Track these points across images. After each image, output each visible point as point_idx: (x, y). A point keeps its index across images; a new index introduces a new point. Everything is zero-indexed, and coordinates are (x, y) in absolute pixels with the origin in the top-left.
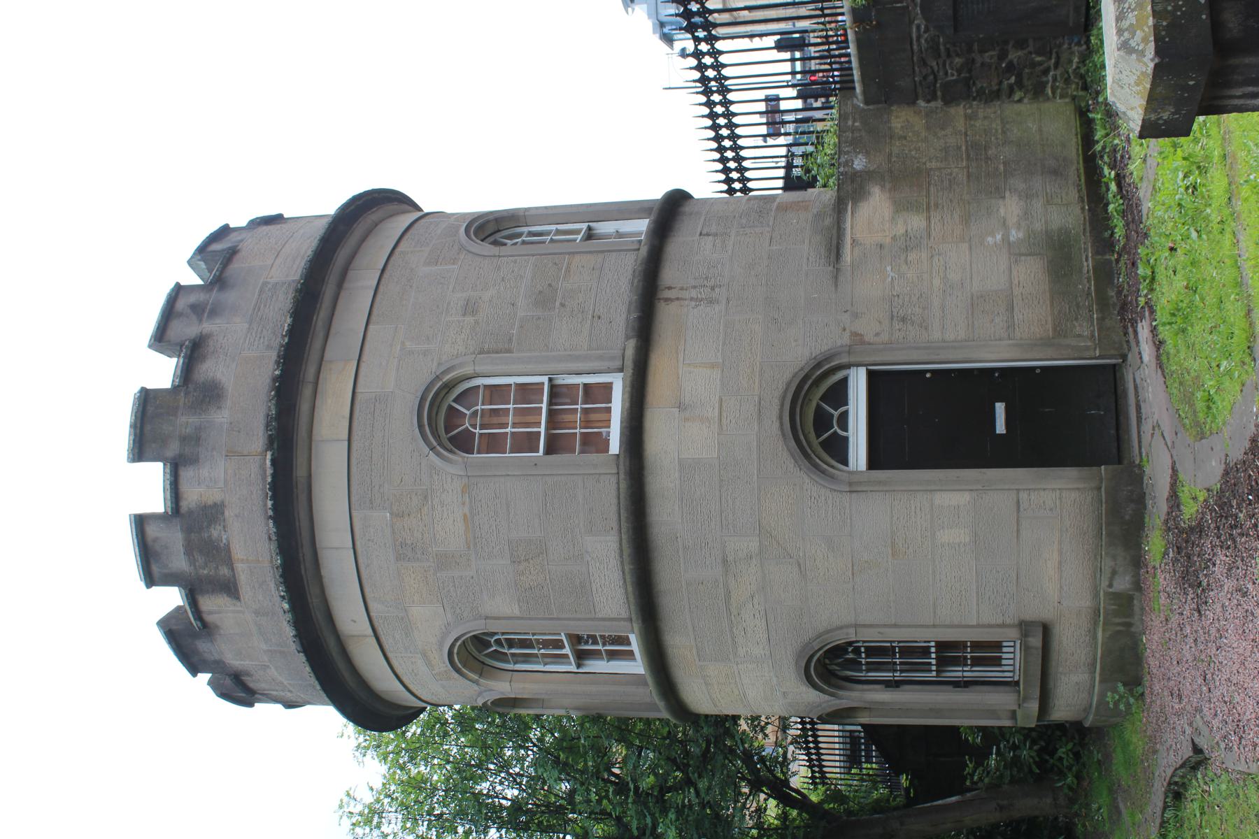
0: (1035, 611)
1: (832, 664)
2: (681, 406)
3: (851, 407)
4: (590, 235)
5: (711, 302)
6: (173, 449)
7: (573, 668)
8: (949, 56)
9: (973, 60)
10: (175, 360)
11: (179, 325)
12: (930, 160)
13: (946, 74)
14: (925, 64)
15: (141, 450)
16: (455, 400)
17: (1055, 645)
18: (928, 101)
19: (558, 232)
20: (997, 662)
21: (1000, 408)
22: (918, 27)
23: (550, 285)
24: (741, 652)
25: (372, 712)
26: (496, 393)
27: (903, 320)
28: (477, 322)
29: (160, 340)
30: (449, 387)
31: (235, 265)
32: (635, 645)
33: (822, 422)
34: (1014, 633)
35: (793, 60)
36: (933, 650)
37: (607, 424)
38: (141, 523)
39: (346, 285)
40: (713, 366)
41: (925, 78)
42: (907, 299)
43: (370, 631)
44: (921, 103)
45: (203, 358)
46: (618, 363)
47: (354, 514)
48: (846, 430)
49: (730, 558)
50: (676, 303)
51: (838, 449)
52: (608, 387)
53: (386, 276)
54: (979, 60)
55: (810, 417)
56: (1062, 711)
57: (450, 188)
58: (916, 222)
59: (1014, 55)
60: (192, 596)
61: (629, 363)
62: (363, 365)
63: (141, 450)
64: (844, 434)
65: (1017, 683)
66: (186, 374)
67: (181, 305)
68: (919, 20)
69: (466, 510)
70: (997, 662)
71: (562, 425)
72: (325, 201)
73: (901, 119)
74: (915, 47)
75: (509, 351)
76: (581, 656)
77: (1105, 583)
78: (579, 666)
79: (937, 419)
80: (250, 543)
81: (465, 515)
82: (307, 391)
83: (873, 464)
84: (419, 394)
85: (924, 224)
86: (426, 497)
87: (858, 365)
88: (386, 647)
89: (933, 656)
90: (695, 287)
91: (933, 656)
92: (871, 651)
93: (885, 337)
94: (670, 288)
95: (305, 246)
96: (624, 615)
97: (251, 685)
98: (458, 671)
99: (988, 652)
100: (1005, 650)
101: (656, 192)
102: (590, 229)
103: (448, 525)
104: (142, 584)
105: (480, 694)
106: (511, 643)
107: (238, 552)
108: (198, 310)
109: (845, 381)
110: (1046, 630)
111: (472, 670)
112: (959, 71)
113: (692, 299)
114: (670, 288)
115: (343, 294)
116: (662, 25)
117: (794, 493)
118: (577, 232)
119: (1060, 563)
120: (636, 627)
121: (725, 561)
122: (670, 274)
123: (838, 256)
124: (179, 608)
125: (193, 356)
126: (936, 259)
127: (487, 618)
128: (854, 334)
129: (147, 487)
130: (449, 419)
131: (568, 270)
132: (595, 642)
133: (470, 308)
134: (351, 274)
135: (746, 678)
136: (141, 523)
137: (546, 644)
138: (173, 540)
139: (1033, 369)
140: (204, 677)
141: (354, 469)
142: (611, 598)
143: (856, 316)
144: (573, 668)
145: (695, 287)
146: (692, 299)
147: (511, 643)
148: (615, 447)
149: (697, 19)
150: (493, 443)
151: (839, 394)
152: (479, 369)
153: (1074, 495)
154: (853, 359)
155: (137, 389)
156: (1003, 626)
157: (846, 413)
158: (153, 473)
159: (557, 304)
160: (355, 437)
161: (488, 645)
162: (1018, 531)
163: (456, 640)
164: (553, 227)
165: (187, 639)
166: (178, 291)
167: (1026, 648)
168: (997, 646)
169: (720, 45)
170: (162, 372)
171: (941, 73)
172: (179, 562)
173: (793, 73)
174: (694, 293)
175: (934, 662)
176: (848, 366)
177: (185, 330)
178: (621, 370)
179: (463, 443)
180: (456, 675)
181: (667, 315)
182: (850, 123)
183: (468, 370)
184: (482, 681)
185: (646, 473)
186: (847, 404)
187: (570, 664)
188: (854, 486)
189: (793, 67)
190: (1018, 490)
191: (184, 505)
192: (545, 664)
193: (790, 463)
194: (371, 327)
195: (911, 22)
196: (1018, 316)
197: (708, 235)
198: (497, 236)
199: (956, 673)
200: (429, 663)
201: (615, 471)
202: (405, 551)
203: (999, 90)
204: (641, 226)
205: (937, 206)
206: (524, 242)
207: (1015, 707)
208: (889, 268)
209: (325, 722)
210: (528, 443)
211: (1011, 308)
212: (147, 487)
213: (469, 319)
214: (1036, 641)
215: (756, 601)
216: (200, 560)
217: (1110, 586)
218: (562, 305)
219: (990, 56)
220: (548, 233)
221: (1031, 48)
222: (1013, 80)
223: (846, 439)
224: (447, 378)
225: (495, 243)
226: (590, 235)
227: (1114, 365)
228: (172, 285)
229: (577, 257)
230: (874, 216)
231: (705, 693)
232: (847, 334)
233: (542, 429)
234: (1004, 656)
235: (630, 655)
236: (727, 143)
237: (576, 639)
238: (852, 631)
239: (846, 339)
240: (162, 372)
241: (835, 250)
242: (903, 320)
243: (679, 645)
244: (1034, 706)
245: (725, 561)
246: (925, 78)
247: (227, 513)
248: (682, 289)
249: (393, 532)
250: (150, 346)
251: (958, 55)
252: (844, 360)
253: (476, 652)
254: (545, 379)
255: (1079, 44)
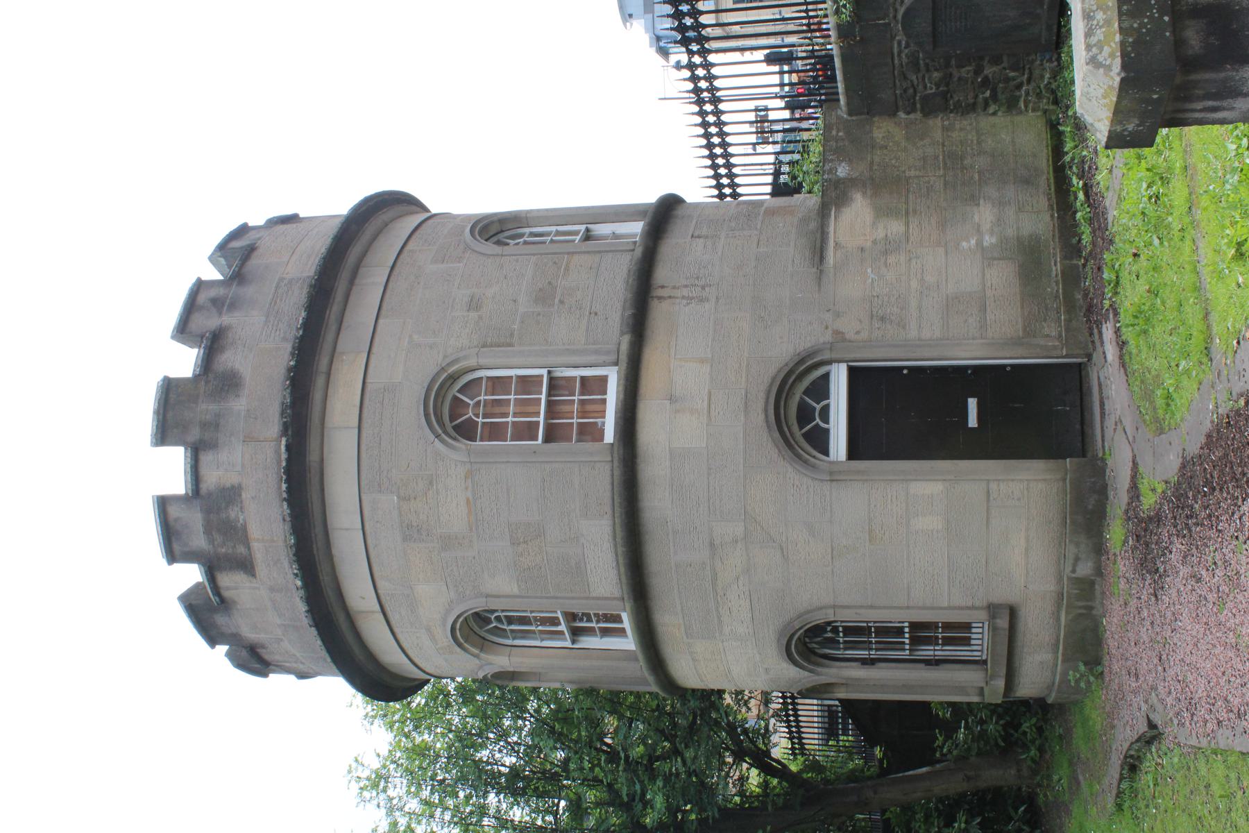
0: (1002, 595)
1: (812, 642)
2: (672, 399)
3: (832, 401)
4: (588, 237)
5: (702, 300)
6: (195, 434)
7: (568, 644)
8: (928, 70)
9: (951, 74)
10: (196, 350)
11: (202, 318)
12: (910, 169)
13: (925, 87)
14: (905, 78)
15: (164, 434)
16: (459, 391)
17: (1021, 627)
18: (908, 113)
19: (558, 233)
20: (966, 641)
21: (972, 403)
22: (899, 43)
23: (550, 283)
24: (726, 630)
25: (380, 684)
26: (498, 384)
27: (882, 319)
28: (480, 317)
29: (183, 331)
30: (453, 378)
31: (254, 262)
32: (627, 623)
33: (805, 415)
34: (983, 615)
35: (782, 73)
36: (907, 630)
37: (602, 414)
38: (163, 504)
39: (357, 281)
40: (702, 361)
41: (905, 91)
42: (886, 299)
43: (378, 608)
44: (902, 115)
45: (222, 350)
46: (613, 358)
47: (363, 497)
48: (827, 422)
49: (717, 542)
50: (669, 301)
51: (819, 440)
52: (604, 380)
53: (395, 273)
54: (956, 74)
55: (792, 411)
56: (1027, 688)
57: (457, 189)
58: (896, 227)
59: (989, 71)
60: (211, 572)
61: (624, 358)
62: (373, 357)
63: (164, 434)
64: (825, 426)
65: (985, 662)
66: (207, 364)
67: (202, 298)
68: (901, 37)
69: (469, 494)
70: (966, 641)
71: (560, 415)
72: (334, 200)
73: (882, 129)
74: (896, 62)
75: (510, 345)
76: (576, 633)
77: (1068, 569)
78: (573, 642)
79: (910, 412)
80: (265, 523)
81: (468, 500)
82: (320, 381)
83: (853, 454)
84: (426, 385)
85: (902, 229)
86: (431, 483)
87: (839, 361)
88: (393, 623)
89: (907, 635)
90: (686, 286)
91: (907, 635)
92: (849, 631)
93: (864, 335)
94: (663, 287)
95: (319, 245)
96: (617, 594)
97: (266, 657)
98: (460, 645)
99: (958, 632)
100: (974, 630)
101: (650, 197)
102: (588, 230)
103: (451, 507)
104: (164, 561)
105: (481, 667)
106: (510, 620)
107: (254, 532)
108: (217, 303)
109: (826, 377)
110: (1013, 612)
111: (474, 645)
112: (938, 86)
113: (683, 297)
114: (663, 287)
115: (354, 289)
116: (658, 39)
117: (779, 485)
118: (576, 233)
119: (1027, 550)
120: (628, 605)
121: (712, 545)
122: (663, 274)
123: (822, 258)
124: (198, 585)
125: (213, 347)
126: (914, 262)
127: (487, 596)
128: (836, 332)
129: (169, 470)
130: (455, 410)
131: (567, 269)
132: (589, 620)
133: (474, 304)
134: (362, 271)
135: (730, 655)
136: (163, 504)
137: (544, 621)
138: (194, 519)
139: (1004, 366)
140: (222, 649)
141: (363, 455)
142: (604, 578)
143: (838, 315)
144: (568, 644)
145: (686, 286)
146: (683, 297)
147: (510, 620)
148: (609, 436)
149: (691, 34)
150: (495, 432)
151: (821, 389)
152: (482, 361)
153: (1041, 485)
154: (834, 356)
155: (160, 377)
156: (973, 608)
157: (827, 406)
158: (175, 457)
159: (556, 301)
160: (365, 425)
161: (488, 621)
162: (988, 519)
163: (458, 617)
164: (553, 229)
165: (207, 612)
166: (200, 286)
167: (994, 629)
168: (967, 627)
169: (712, 58)
170: (183, 361)
171: (920, 87)
172: (199, 541)
173: (782, 85)
174: (685, 292)
175: (907, 641)
176: (829, 362)
177: (206, 322)
178: (616, 364)
179: (466, 431)
180: (458, 650)
181: (659, 312)
182: (834, 133)
183: (472, 362)
184: (482, 655)
185: (639, 461)
186: (828, 398)
187: (565, 640)
188: (835, 475)
189: (782, 79)
190: (988, 481)
191: (204, 488)
192: (542, 640)
193: (774, 453)
194: (381, 321)
195: (893, 38)
196: (990, 316)
197: (699, 237)
198: (501, 236)
199: (927, 651)
200: (433, 638)
201: (609, 459)
202: (411, 532)
203: (975, 104)
204: (636, 228)
205: (915, 212)
206: (526, 243)
207: (983, 685)
208: (869, 270)
209: (335, 690)
210: (527, 431)
211: (983, 309)
212: (169, 470)
213: (473, 315)
214: (1003, 623)
215: (740, 583)
216: (219, 539)
217: (1074, 571)
218: (561, 302)
219: (968, 71)
220: (548, 234)
221: (1005, 64)
222: (988, 94)
223: (827, 431)
224: (451, 370)
225: (499, 243)
226: (588, 237)
227: (1080, 364)
228: (194, 280)
229: (576, 257)
230: (856, 221)
231: (690, 670)
232: (830, 332)
233: (541, 419)
234: (974, 636)
235: (622, 632)
236: (711, 119)
237: (571, 617)
238: (831, 611)
239: (828, 337)
240: (183, 361)
241: (818, 253)
242: (882, 319)
243: (668, 623)
244: (1000, 683)
245: (712, 545)
246: (905, 91)
247: (244, 495)
248: (674, 287)
249: (400, 515)
250: (173, 337)
251: (936, 70)
252: (826, 356)
253: (477, 628)
254: (544, 372)
255: (1050, 60)
